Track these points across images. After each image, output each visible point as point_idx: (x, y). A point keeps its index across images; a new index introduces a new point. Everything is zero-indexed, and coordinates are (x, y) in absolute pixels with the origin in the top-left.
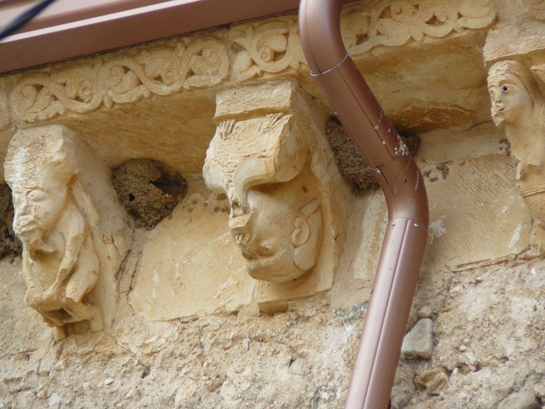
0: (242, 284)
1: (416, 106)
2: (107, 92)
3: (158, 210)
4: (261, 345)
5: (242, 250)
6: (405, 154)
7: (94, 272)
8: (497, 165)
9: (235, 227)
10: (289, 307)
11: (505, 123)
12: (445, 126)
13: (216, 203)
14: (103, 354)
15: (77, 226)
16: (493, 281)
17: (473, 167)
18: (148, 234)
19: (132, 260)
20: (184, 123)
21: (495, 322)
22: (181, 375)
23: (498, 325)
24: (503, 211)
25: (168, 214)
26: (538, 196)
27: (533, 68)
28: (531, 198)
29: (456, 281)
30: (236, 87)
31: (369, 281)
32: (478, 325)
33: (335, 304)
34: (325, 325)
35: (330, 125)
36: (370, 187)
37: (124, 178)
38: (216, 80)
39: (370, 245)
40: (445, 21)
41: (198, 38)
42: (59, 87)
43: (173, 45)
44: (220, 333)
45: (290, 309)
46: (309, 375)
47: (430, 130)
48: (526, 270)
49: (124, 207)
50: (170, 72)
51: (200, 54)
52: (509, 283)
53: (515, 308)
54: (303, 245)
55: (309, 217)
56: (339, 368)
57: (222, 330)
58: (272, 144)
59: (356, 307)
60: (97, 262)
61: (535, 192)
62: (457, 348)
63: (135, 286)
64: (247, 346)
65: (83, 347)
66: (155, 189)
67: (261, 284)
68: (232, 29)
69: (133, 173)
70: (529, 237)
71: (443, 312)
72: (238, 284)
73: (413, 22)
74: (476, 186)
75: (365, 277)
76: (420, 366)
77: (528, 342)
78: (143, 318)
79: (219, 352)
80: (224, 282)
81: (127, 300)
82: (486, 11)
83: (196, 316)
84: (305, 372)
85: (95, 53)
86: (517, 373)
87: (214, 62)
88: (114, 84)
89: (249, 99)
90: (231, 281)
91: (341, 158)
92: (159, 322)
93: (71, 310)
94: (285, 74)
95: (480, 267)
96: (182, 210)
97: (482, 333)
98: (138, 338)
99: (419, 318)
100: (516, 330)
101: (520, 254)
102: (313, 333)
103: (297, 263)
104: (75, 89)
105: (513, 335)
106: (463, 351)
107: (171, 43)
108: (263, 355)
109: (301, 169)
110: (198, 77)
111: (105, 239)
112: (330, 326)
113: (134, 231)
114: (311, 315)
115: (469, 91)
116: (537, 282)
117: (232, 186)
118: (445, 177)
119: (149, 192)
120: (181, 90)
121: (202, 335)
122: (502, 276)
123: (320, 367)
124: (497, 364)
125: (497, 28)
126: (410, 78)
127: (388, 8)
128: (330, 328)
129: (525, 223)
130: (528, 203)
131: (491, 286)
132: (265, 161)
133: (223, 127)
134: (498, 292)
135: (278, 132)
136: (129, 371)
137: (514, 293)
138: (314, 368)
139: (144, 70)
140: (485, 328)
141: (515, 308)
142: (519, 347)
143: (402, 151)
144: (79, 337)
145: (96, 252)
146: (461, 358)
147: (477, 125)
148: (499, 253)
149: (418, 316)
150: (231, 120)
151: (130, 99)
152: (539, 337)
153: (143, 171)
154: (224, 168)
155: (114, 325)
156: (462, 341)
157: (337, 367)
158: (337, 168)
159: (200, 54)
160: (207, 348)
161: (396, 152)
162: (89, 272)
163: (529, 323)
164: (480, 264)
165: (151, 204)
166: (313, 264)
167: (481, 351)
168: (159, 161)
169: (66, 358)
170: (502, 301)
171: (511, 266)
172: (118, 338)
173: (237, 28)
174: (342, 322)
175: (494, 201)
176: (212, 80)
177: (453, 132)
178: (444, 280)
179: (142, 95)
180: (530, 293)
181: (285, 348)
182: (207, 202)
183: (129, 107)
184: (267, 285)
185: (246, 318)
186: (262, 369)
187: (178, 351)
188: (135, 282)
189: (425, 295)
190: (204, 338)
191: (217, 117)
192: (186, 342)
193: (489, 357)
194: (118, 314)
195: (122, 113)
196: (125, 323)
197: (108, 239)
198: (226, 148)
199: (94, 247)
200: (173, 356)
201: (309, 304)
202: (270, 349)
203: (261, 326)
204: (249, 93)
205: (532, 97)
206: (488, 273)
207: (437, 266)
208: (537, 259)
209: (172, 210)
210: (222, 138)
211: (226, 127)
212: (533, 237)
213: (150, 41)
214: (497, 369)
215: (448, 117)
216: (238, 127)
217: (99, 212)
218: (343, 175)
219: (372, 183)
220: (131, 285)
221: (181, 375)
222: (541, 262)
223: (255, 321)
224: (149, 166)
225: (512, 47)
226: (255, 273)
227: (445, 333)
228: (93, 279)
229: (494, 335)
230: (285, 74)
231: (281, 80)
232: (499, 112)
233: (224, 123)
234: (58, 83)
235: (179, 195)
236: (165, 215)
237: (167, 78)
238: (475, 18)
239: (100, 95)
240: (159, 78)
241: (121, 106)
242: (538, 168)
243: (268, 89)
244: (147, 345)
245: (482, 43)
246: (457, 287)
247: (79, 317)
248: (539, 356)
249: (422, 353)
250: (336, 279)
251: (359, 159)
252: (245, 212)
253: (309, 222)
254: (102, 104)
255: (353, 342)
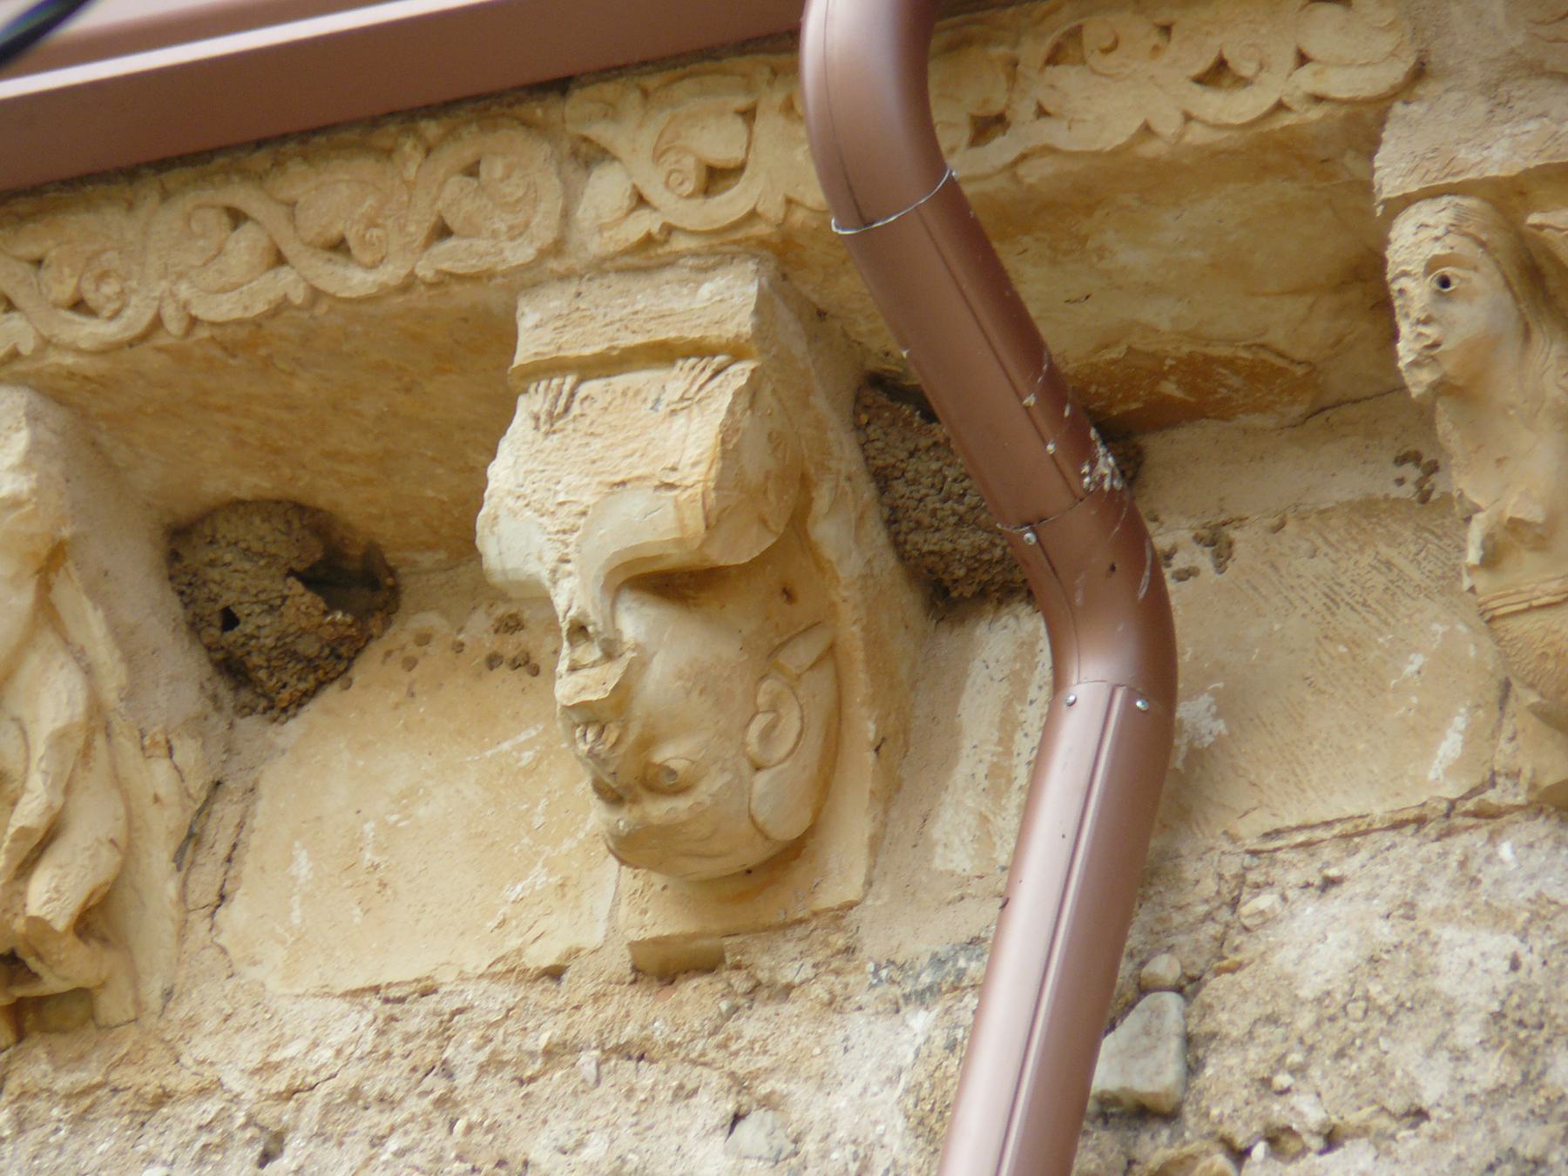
0: (576, 886)
1: (1139, 346)
2: (174, 288)
3: (310, 660)
4: (637, 1070)
5: (594, 772)
6: (1112, 486)
7: (112, 841)
8: (1389, 531)
9: (576, 701)
10: (727, 955)
11: (1441, 388)
12: (1223, 411)
13: (490, 643)
14: (136, 1093)
15: (64, 697)
16: (1379, 882)
17: (1312, 535)
18: (278, 734)
19: (227, 811)
20: (408, 390)
21: (1387, 1004)
22: (383, 1158)
23: (1396, 1013)
24: (1410, 669)
25: (340, 674)
26: (1536, 616)
27: (1534, 219)
28: (1511, 623)
29: (1261, 879)
30: (581, 277)
31: (981, 877)
32: (1331, 1011)
33: (873, 947)
34: (841, 1011)
35: (869, 401)
36: (982, 594)
37: (206, 559)
38: (520, 253)
39: (982, 771)
40: (1256, 75)
41: (468, 122)
42: (22, 270)
43: (387, 142)
44: (506, 1034)
45: (729, 961)
46: (794, 1161)
47: (1174, 423)
48: (1483, 846)
49: (203, 652)
50: (376, 226)
51: (472, 171)
52: (1430, 886)
53: (1451, 963)
54: (781, 762)
55: (799, 677)
56: (886, 1140)
57: (511, 1025)
58: (699, 446)
59: (942, 956)
60: (121, 811)
61: (1525, 606)
62: (1266, 1082)
63: (235, 891)
64: (594, 1072)
65: (73, 1071)
66: (303, 595)
67: (639, 883)
68: (577, 95)
69: (236, 544)
70: (1494, 747)
71: (1218, 972)
72: (562, 885)
73: (1152, 77)
74: (1320, 595)
75: (968, 868)
76: (1145, 1137)
77: (1493, 1065)
78: (263, 985)
79: (501, 1092)
80: (520, 880)
81: (211, 930)
82: (1386, 43)
83: (429, 983)
84: (780, 1152)
85: (138, 165)
86: (1459, 1158)
87: (514, 198)
88: (199, 263)
89: (625, 312)
90: (539, 878)
91: (900, 502)
92: (313, 1000)
93: (39, 957)
94: (739, 235)
95: (1335, 837)
96: (384, 662)
97: (1345, 1037)
98: (246, 1046)
99: (1143, 989)
100: (1452, 1029)
101: (1464, 798)
102: (804, 1035)
103: (760, 819)
104: (72, 276)
105: (1445, 1044)
106: (1285, 1092)
107: (383, 138)
108: (645, 1100)
109: (781, 530)
110: (464, 243)
111: (147, 742)
112: (857, 1013)
113: (231, 726)
114: (797, 980)
115: (1309, 299)
116: (1517, 885)
117: (570, 574)
118: (1220, 568)
119: (283, 603)
120: (408, 285)
121: (449, 1038)
122: (1408, 867)
123: (826, 1137)
124: (1390, 1131)
125: (1420, 99)
126: (1131, 257)
127: (1075, 34)
128: (859, 1019)
129: (1478, 706)
130: (1502, 639)
131: (1370, 897)
132: (676, 499)
133: (540, 397)
134: (1395, 913)
135: (716, 411)
136: (218, 1146)
137: (1447, 915)
138: (808, 1138)
139: (292, 218)
140: (1355, 1021)
141: (1451, 963)
142: (1462, 1080)
143: (1103, 477)
144: (58, 1041)
145: (118, 781)
146: (1278, 1111)
147: (1322, 410)
148: (1398, 794)
149: (1139, 985)
150: (565, 376)
151: (246, 308)
152: (1525, 1051)
153: (269, 539)
154: (545, 520)
155: (171, 1005)
156: (1281, 1059)
157: (882, 1135)
158: (884, 535)
159: (472, 171)
160: (464, 1079)
161: (1087, 480)
162: (98, 840)
163: (1495, 1007)
164: (1337, 829)
165: (288, 640)
166: (806, 824)
167: (1340, 1090)
168: (319, 510)
169: (16, 1106)
170: (1407, 941)
171: (1433, 834)
172: (181, 1046)
173: (592, 91)
174: (897, 1003)
175: (1381, 640)
176: (507, 254)
177: (1245, 431)
178: (1221, 877)
179: (285, 298)
180: (1499, 918)
181: (714, 1079)
182: (461, 637)
183: (242, 333)
184: (658, 888)
185: (588, 988)
186: (642, 1140)
187: (373, 1086)
188: (235, 877)
189: (1161, 920)
190: (457, 1048)
191: (521, 366)
192: (398, 1059)
193: (1367, 1111)
194: (183, 973)
195: (217, 352)
196: (206, 999)
197: (155, 744)
198: (552, 459)
199: (114, 767)
200: (356, 1100)
201: (791, 945)
202: (666, 1082)
203: (638, 1012)
204: (622, 294)
205: (1525, 310)
206: (1362, 856)
207: (1200, 836)
208: (1516, 816)
209: (351, 660)
210: (537, 428)
211: (550, 396)
212: (1504, 745)
213: (315, 132)
214: (1394, 1145)
215: (1235, 381)
216: (586, 398)
217: (130, 661)
218: (902, 557)
219: (992, 582)
220: (223, 886)
221: (383, 1158)
222: (1530, 824)
223: (617, 997)
224: (289, 523)
225: (1466, 155)
226: (628, 849)
227: (1227, 1035)
228: (108, 862)
229: (1384, 1044)
230: (739, 235)
231: (725, 254)
232: (1426, 353)
233: (544, 384)
234: (19, 259)
235: (373, 615)
236: (332, 675)
237: (366, 244)
238: (1349, 65)
239: (153, 295)
240: (339, 247)
241: (216, 332)
242: (1538, 531)
243: (683, 282)
244: (277, 1067)
245: (1370, 144)
246: (1261, 897)
247: (65, 979)
248: (1529, 1106)
249: (1155, 1095)
250: (876, 872)
251: (956, 506)
252: (609, 655)
253: (801, 692)
254: (157, 323)
255: (934, 1061)
